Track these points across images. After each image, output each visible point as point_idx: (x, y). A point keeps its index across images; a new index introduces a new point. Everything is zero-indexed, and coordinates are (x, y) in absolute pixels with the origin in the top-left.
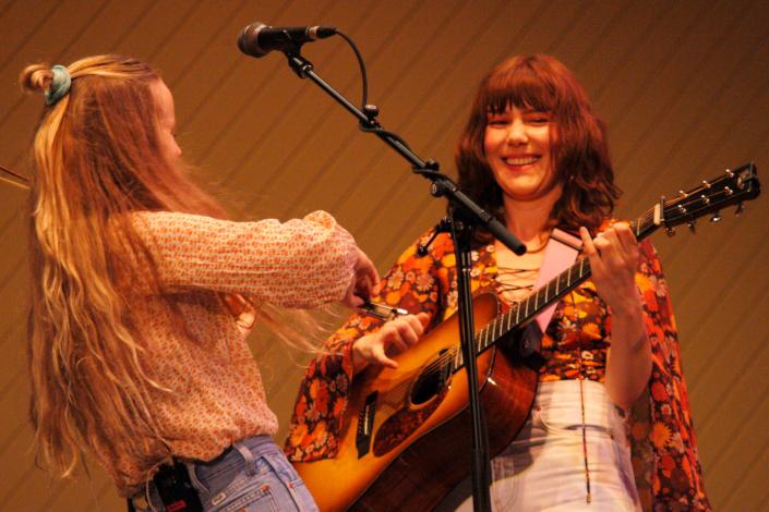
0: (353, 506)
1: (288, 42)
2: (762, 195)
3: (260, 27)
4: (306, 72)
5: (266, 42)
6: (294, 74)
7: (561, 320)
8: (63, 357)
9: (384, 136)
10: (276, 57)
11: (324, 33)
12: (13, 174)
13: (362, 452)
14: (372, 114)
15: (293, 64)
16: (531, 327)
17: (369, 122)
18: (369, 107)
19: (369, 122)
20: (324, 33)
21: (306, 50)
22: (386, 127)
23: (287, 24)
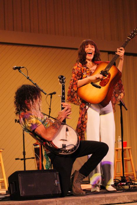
0: (65, 120)
1: (19, 68)
2: (67, 92)
3: (15, 66)
4: (21, 72)
5: (16, 68)
6: (19, 72)
7: (47, 154)
8: (120, 53)
9: (30, 80)
10: (17, 70)
11: (23, 67)
12: (131, 137)
13: (65, 102)
14: (28, 77)
15: (20, 71)
16: (128, 150)
17: (28, 78)
18: (28, 76)
19: (28, 78)
20: (23, 67)
21: (21, 69)
22: (30, 79)
23: (18, 66)
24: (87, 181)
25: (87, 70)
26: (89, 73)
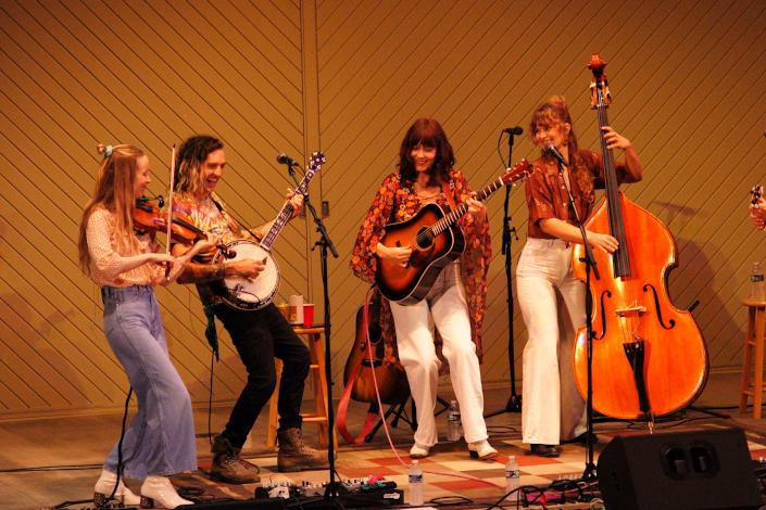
25: (411, 197)
26: (412, 208)
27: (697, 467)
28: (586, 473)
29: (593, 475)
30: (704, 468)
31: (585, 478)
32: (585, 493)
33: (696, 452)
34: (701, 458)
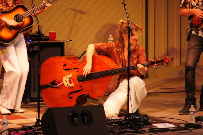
24: (12, 131)
27: (84, 121)
28: (36, 123)
29: (39, 124)
30: (86, 121)
31: (36, 125)
32: (35, 132)
33: (83, 115)
34: (85, 117)
